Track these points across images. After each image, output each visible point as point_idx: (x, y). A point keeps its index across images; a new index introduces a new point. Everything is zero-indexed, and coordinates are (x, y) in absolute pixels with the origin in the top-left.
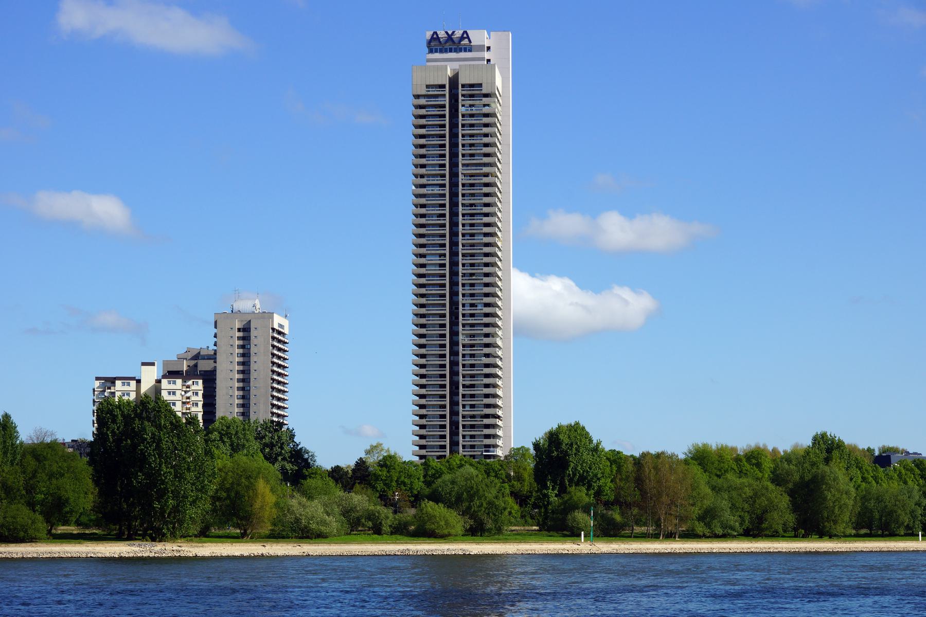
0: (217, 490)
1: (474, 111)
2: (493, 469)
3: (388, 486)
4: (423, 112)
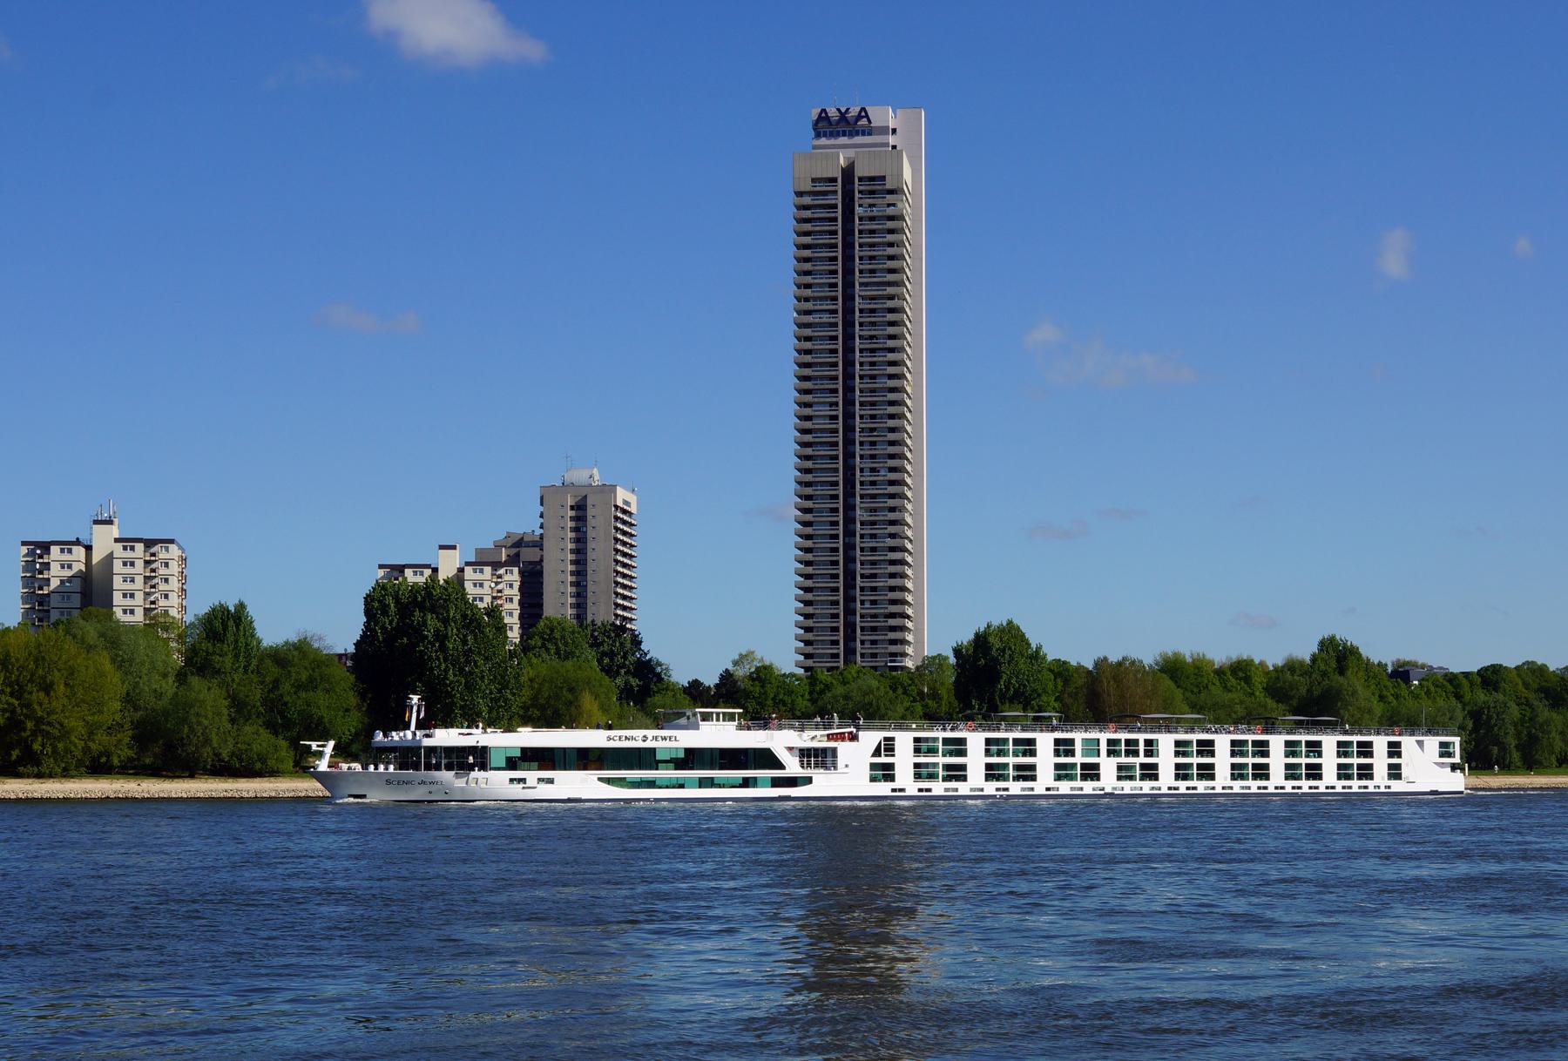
1: (875, 212)
4: (807, 214)
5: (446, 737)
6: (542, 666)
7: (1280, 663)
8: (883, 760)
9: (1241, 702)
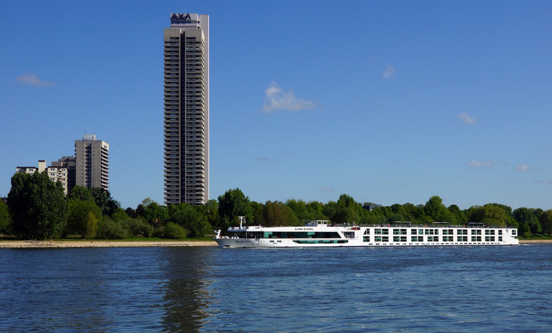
0: (70, 217)
1: (192, 49)
2: (200, 209)
3: (153, 216)
4: (169, 49)
5: (252, 229)
6: (76, 202)
7: (327, 203)
8: (367, 235)
9: (314, 216)
